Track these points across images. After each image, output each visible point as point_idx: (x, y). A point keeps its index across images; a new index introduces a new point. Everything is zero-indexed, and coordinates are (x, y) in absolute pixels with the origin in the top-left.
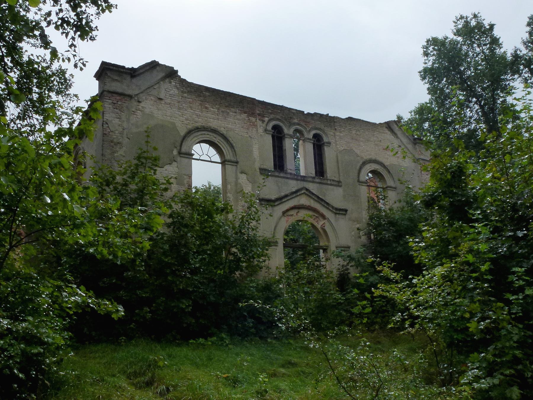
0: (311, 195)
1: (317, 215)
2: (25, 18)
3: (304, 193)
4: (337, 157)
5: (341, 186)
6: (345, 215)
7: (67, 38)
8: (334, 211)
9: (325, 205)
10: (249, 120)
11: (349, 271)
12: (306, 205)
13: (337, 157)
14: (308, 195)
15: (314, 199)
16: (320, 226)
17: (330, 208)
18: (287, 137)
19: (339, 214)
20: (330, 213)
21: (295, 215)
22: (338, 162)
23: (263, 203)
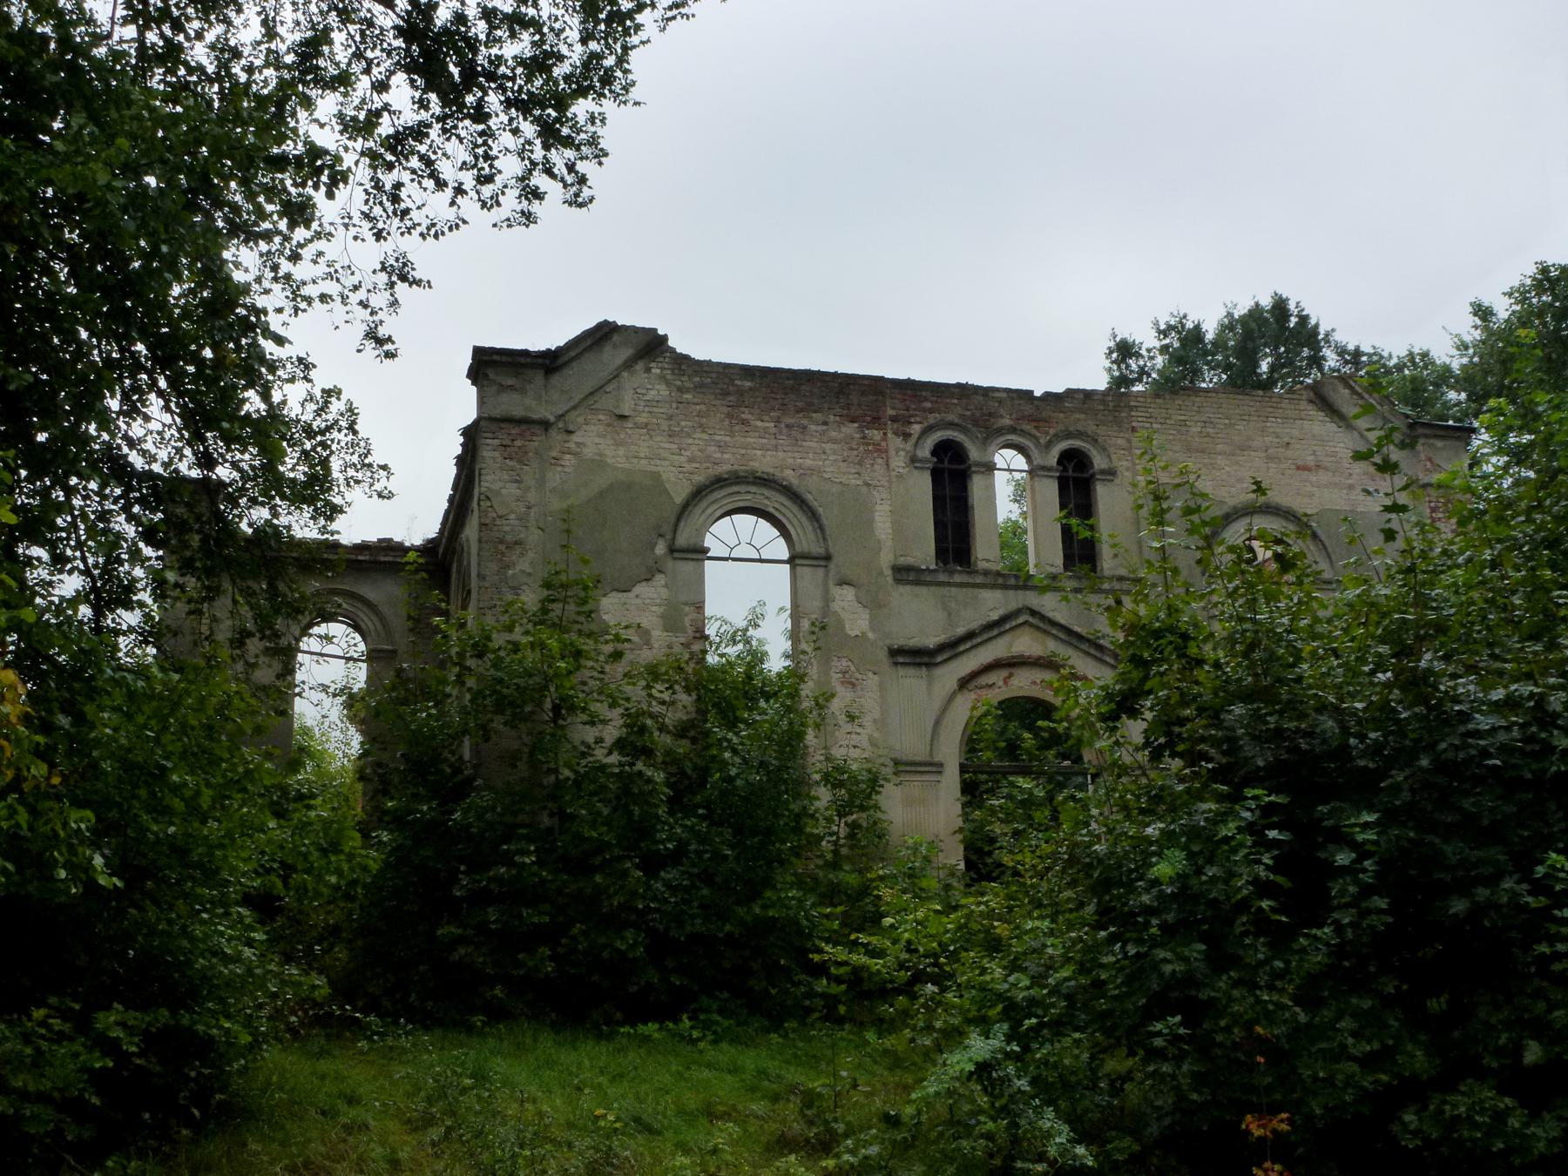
3: (1026, 623)
9: (1092, 651)
10: (864, 437)
14: (1038, 628)
15: (1056, 637)
21: (1001, 683)
23: (901, 660)
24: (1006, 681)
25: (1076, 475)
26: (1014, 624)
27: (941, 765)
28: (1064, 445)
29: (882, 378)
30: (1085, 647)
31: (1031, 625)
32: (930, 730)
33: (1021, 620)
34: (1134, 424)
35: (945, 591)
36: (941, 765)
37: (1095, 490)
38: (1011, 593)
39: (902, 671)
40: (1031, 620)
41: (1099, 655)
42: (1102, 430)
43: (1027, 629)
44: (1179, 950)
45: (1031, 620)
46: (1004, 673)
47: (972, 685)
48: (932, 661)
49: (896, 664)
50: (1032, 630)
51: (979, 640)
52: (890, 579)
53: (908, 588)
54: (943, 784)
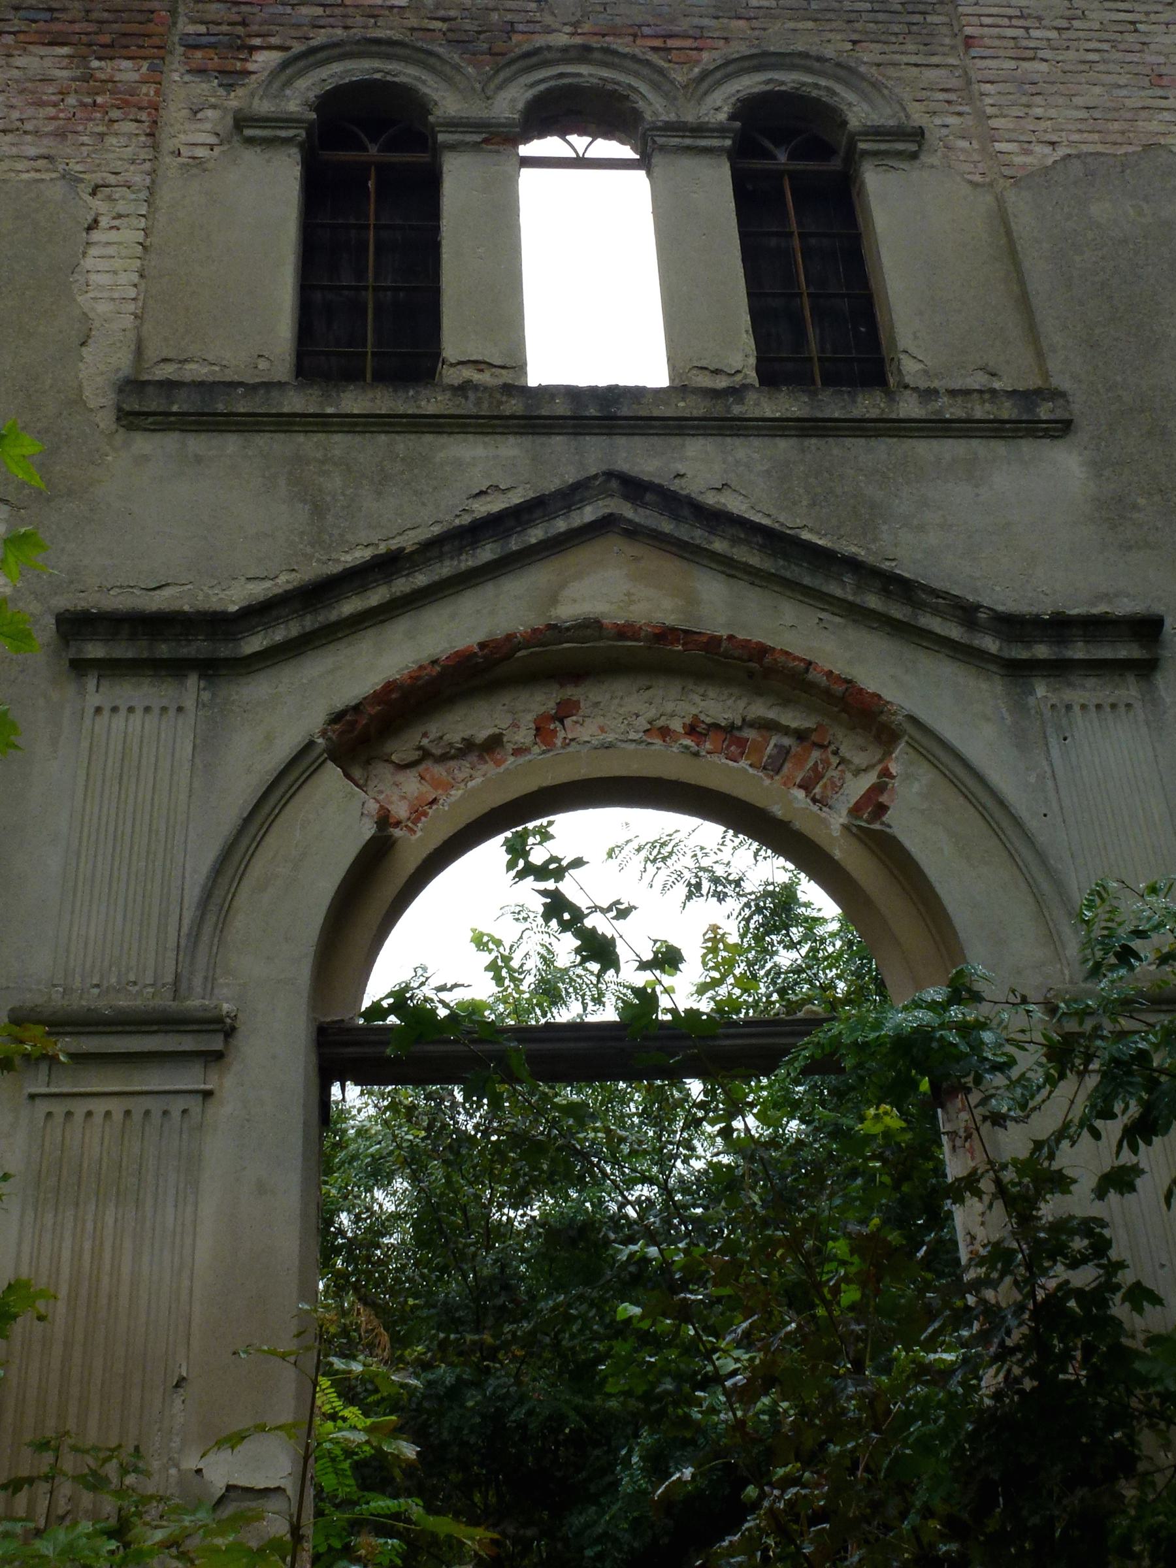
0: (698, 535)
1: (792, 719)
2: (665, 1540)
3: (604, 526)
4: (1002, 218)
5: (1062, 428)
6: (1146, 669)
7: (1086, 979)
8: (991, 644)
9: (873, 601)
10: (87, 77)
11: (513, 873)
12: (625, 632)
13: (1002, 218)
14: (657, 539)
15: (729, 567)
16: (838, 819)
17: (936, 624)
18: (453, 147)
19: (1058, 669)
20: (947, 670)
21: (524, 735)
22: (1012, 252)
23: (95, 650)
24: (541, 731)
25: (800, 165)
26: (561, 525)
27: (226, 1028)
28: (750, 83)
29: (644, 388)
30: (842, 588)
31: (633, 532)
32: (193, 894)
33: (589, 514)
34: (969, 31)
35: (309, 444)
36: (226, 1028)
37: (863, 184)
38: (558, 442)
39: (95, 694)
40: (628, 511)
41: (898, 612)
42: (869, 54)
43: (614, 546)
44: (580, 1321)
45: (628, 511)
46: (541, 701)
47: (402, 748)
48: (224, 651)
49: (80, 667)
50: (632, 549)
51: (421, 579)
52: (106, 420)
53: (170, 441)
54: (226, 1109)
